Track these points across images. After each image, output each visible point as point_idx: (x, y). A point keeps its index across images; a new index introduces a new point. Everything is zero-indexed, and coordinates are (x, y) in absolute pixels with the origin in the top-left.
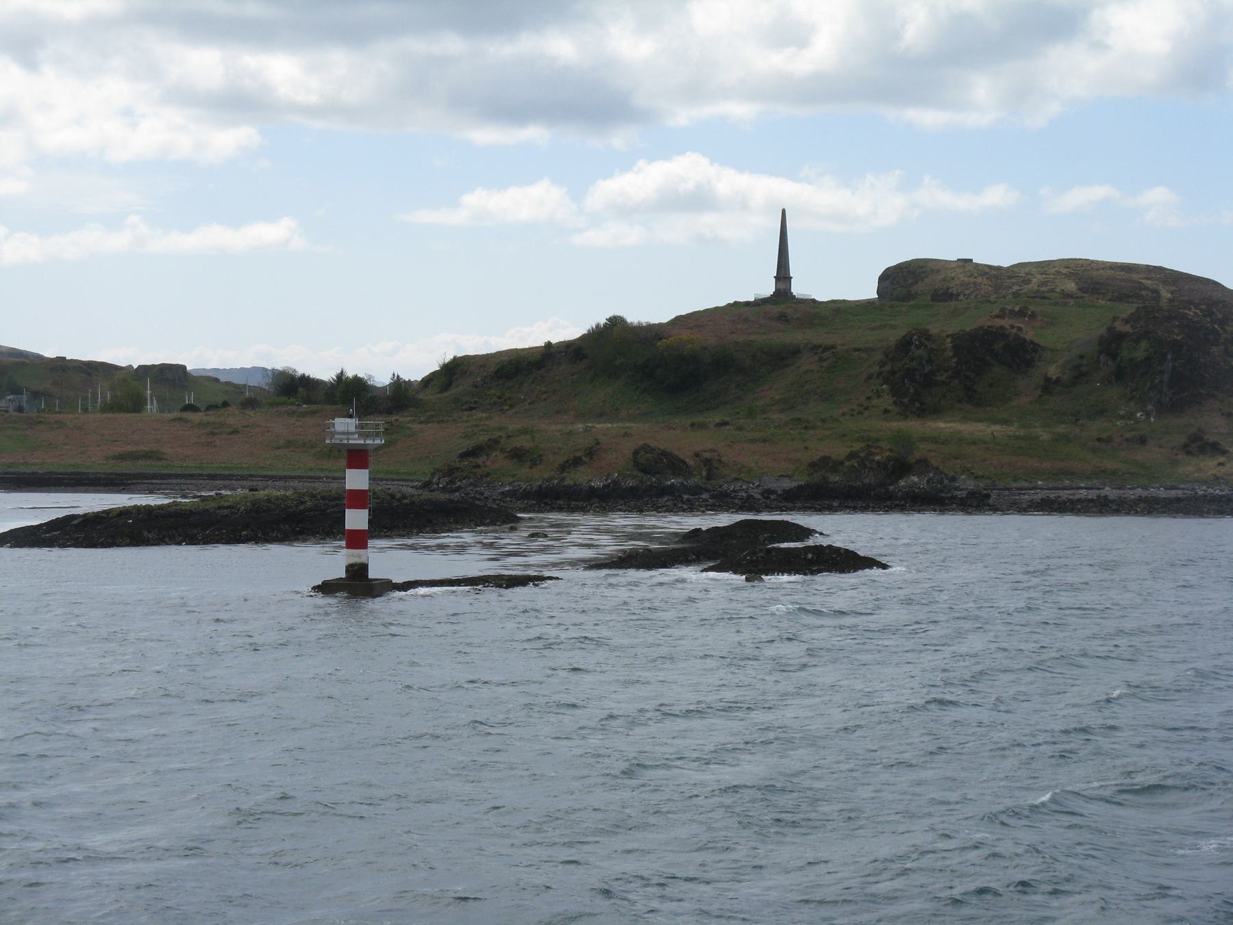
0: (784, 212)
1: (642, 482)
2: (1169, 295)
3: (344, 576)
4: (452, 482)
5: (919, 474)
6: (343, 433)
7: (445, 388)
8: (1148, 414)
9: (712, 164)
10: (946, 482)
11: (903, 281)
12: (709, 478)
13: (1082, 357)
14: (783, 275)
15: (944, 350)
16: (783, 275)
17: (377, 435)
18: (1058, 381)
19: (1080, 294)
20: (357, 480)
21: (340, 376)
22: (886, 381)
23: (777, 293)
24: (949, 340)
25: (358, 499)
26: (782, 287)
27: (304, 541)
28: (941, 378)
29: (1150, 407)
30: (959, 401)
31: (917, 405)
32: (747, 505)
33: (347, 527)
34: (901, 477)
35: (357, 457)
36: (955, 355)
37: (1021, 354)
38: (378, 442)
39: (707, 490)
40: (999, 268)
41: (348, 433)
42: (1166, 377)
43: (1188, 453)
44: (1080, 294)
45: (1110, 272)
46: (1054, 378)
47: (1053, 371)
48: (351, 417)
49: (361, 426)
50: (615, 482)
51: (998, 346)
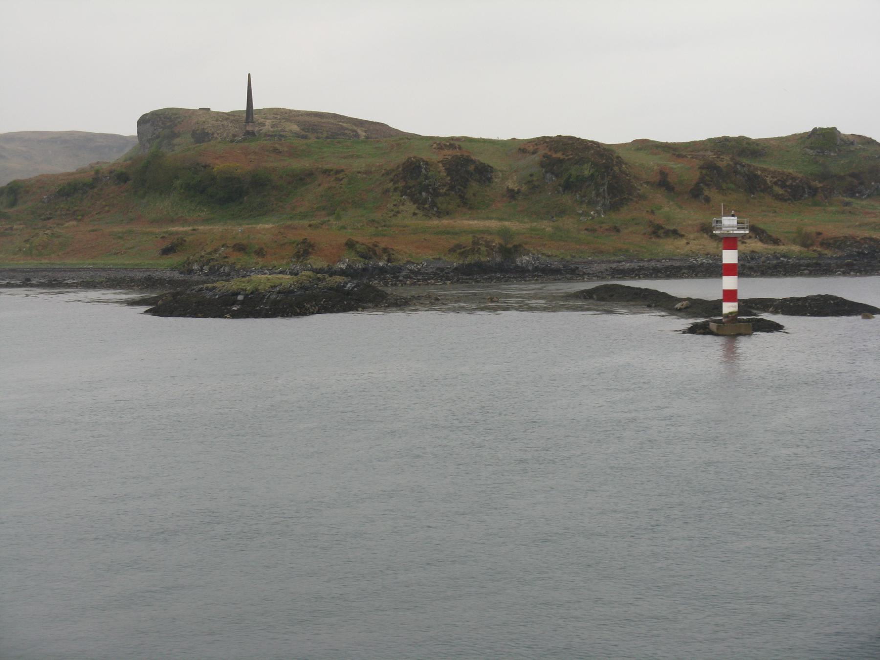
0: (249, 75)
2: (364, 134)
6: (729, 227)
8: (598, 212)
12: (389, 261)
13: (531, 175)
15: (439, 172)
18: (519, 192)
19: (303, 133)
22: (403, 193)
24: (441, 165)
27: (364, 308)
28: (443, 191)
29: (598, 208)
30: (459, 206)
31: (435, 209)
32: (600, 276)
36: (448, 175)
37: (484, 173)
43: (658, 237)
44: (303, 133)
45: (317, 119)
46: (516, 189)
47: (511, 184)
48: (733, 216)
51: (471, 168)
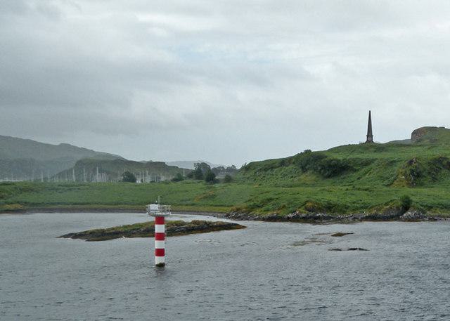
4: (237, 214)
14: (370, 134)
16: (370, 134)
34: (404, 213)
50: (298, 215)
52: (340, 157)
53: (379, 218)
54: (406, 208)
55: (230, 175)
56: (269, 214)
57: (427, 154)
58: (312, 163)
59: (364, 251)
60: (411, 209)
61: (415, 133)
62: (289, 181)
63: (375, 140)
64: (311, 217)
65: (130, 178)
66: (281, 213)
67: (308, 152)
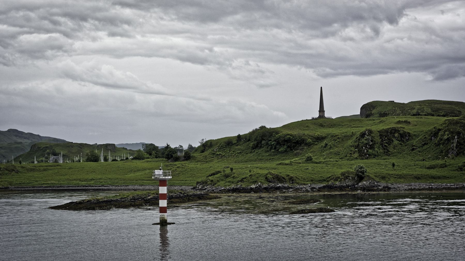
0: (321, 88)
1: (269, 186)
3: (359, 113)
4: (204, 187)
5: (366, 181)
7: (203, 152)
9: (168, 147)
10: (376, 183)
11: (368, 109)
14: (322, 110)
16: (322, 110)
17: (169, 175)
20: (163, 190)
21: (168, 147)
23: (320, 117)
25: (163, 197)
26: (321, 114)
33: (160, 206)
34: (360, 182)
35: (163, 183)
38: (169, 177)
39: (291, 188)
40: (403, 104)
41: (160, 175)
42: (455, 145)
48: (160, 169)
49: (164, 173)
50: (260, 186)
52: (295, 132)
53: (336, 187)
54: (361, 178)
55: (189, 155)
56: (233, 186)
57: (377, 126)
58: (265, 141)
59: (172, 225)
60: (366, 179)
61: (364, 108)
62: (427, 164)
63: (327, 115)
64: (272, 187)
65: (95, 159)
66: (111, 187)
67: (263, 128)
